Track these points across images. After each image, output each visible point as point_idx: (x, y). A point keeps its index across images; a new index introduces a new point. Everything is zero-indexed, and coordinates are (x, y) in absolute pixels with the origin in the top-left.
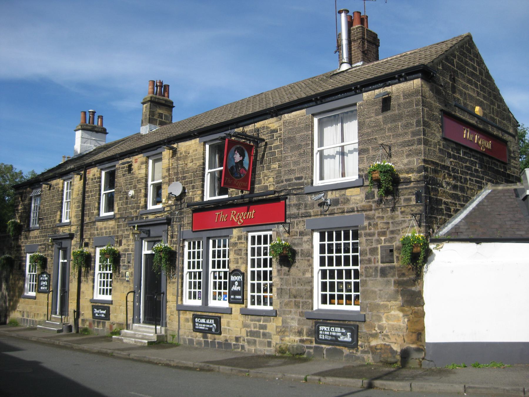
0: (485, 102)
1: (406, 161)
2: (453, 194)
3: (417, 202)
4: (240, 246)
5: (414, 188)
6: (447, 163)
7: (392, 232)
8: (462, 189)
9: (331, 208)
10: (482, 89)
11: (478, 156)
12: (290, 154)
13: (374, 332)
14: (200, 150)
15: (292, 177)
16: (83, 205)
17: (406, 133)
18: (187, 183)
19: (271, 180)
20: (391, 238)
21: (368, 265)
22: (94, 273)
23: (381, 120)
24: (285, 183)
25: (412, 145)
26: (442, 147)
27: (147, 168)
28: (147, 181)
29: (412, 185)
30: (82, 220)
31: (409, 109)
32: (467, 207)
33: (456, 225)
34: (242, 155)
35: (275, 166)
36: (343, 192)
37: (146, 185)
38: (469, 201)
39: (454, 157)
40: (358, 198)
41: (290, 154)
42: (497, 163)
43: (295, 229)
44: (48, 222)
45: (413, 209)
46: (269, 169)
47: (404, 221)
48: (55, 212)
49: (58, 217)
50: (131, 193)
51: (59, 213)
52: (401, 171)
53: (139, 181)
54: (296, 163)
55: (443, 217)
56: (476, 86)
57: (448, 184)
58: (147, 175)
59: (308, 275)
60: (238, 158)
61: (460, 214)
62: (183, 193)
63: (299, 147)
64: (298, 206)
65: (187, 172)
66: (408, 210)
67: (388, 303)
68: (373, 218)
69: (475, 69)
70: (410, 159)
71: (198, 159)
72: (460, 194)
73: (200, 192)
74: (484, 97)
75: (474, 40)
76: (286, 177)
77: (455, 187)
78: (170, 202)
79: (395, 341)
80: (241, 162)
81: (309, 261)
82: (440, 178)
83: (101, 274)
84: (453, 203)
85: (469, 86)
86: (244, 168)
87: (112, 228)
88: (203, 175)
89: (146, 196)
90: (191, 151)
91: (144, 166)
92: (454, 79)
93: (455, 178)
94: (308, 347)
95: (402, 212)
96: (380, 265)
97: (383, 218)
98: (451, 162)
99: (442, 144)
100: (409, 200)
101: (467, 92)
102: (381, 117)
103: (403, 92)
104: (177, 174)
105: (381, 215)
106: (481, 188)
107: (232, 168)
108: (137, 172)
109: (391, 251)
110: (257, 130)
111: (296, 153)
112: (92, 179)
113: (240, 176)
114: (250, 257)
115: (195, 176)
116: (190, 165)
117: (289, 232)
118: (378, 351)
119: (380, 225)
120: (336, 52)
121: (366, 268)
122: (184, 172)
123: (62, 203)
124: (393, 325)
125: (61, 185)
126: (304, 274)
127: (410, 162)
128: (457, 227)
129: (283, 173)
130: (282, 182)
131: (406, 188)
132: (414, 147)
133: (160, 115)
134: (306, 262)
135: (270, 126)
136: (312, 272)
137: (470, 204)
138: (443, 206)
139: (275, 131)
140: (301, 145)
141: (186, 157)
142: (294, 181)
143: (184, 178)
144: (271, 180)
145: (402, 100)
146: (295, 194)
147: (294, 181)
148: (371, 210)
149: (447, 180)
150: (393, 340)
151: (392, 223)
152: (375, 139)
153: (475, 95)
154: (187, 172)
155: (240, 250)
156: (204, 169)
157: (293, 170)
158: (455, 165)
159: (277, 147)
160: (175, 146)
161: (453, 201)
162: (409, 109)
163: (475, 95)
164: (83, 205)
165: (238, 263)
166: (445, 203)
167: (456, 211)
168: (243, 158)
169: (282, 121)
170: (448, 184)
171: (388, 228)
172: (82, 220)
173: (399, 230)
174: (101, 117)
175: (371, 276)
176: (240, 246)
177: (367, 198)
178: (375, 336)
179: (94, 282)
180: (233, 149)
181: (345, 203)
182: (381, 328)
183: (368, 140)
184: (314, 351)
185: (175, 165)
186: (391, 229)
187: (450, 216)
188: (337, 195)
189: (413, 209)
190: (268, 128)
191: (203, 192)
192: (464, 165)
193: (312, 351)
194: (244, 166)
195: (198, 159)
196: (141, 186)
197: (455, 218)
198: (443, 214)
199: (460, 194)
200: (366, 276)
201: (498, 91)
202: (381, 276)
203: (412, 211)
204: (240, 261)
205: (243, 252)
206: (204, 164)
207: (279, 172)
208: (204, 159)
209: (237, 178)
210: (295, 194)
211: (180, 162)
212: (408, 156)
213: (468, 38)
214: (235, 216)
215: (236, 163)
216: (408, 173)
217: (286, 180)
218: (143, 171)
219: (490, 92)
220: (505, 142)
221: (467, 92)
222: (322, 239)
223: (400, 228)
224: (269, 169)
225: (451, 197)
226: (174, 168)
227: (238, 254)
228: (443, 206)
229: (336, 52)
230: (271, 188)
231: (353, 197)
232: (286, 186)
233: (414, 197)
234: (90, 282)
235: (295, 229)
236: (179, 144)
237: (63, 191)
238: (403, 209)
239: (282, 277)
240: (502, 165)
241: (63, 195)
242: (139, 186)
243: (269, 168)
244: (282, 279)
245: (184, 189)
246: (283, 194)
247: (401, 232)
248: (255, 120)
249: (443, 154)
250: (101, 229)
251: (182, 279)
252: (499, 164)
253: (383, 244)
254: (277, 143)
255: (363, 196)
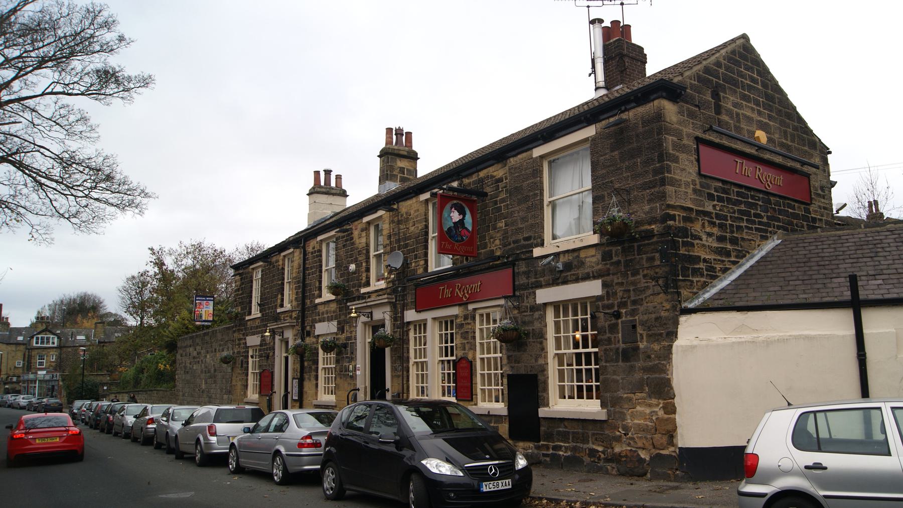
0: (771, 123)
1: (647, 208)
2: (717, 248)
3: (661, 262)
4: (467, 328)
5: (657, 242)
6: (709, 208)
7: (634, 302)
8: (734, 241)
9: (564, 274)
10: (769, 108)
11: (761, 196)
12: (517, 208)
13: (618, 433)
14: (422, 210)
15: (520, 237)
16: (304, 286)
17: (646, 172)
18: (409, 252)
19: (497, 242)
20: (633, 310)
21: (608, 347)
22: (317, 368)
23: (617, 157)
24: (512, 245)
25: (654, 187)
26: (698, 187)
27: (368, 236)
28: (368, 252)
29: (655, 239)
30: (303, 303)
31: (650, 140)
32: (743, 264)
33: (723, 289)
34: (462, 212)
35: (501, 224)
36: (576, 254)
37: (368, 258)
38: (745, 256)
39: (720, 199)
40: (594, 259)
41: (517, 208)
42: (793, 203)
43: (525, 304)
44: (269, 308)
45: (657, 270)
46: (495, 228)
47: (648, 287)
48: (277, 296)
49: (279, 301)
50: (352, 267)
51: (280, 296)
52: (639, 223)
53: (360, 253)
54: (524, 219)
55: (703, 279)
56: (758, 104)
57: (710, 235)
58: (368, 245)
59: (541, 361)
60: (456, 216)
61: (731, 274)
62: (406, 264)
63: (526, 199)
64: (527, 274)
65: (409, 238)
66: (651, 272)
67: (632, 395)
68: (612, 285)
69: (753, 80)
70: (653, 205)
71: (419, 222)
72: (729, 246)
73: (422, 262)
74: (770, 118)
75: (753, 42)
76: (514, 238)
77: (721, 239)
78: (392, 276)
79: (641, 445)
80: (461, 222)
81: (541, 343)
82: (697, 227)
83: (443, 361)
84: (719, 260)
85: (744, 103)
86: (466, 229)
87: (334, 312)
88: (427, 241)
89: (368, 270)
90: (412, 212)
91: (364, 234)
92: (718, 95)
93: (721, 226)
94: (544, 455)
95: (645, 276)
96: (622, 346)
97: (622, 284)
98: (714, 206)
99: (698, 182)
100: (652, 259)
101: (741, 112)
102: (616, 153)
103: (642, 118)
104: (398, 241)
105: (620, 281)
106: (765, 238)
107: (450, 229)
108: (357, 241)
109: (634, 327)
110: (481, 181)
111: (524, 206)
112: (312, 253)
113: (463, 240)
114: (478, 340)
115: (417, 243)
116: (412, 229)
117: (518, 308)
118: (624, 459)
119: (620, 294)
120: (590, 75)
121: (606, 350)
122: (406, 239)
123: (283, 284)
124: (639, 425)
125: (281, 263)
126: (536, 360)
127: (651, 209)
128: (723, 291)
129: (510, 233)
130: (510, 244)
131: (648, 244)
132: (657, 189)
133: (402, 170)
134: (539, 345)
135: (495, 174)
136: (546, 357)
137: (748, 261)
138: (702, 265)
139: (500, 180)
140: (529, 196)
141: (407, 220)
142: (523, 242)
143: (406, 245)
144: (497, 242)
145: (641, 130)
146: (524, 259)
147: (523, 242)
148: (608, 275)
149: (708, 230)
150: (640, 444)
151: (634, 290)
152: (611, 182)
153: (755, 116)
154: (409, 238)
155: (467, 332)
156: (427, 233)
157: (521, 228)
158: (720, 210)
159: (503, 201)
160: (395, 207)
161: (719, 258)
162: (650, 140)
163: (755, 116)
164: (304, 286)
165: (464, 349)
166: (705, 260)
167: (725, 270)
168: (464, 216)
169: (507, 168)
170: (710, 235)
171: (629, 297)
172: (303, 303)
173: (642, 299)
174: (339, 177)
175: (612, 360)
176: (467, 328)
177: (603, 259)
178: (618, 439)
179: (317, 379)
180: (448, 206)
181: (578, 267)
182: (626, 429)
183: (603, 184)
184: (551, 460)
185: (396, 230)
186: (632, 298)
187: (714, 277)
188: (571, 258)
189: (657, 270)
190: (492, 177)
191: (426, 261)
192: (736, 208)
193: (548, 459)
194: (466, 225)
195: (419, 222)
196: (362, 258)
197: (721, 280)
198: (702, 275)
199: (729, 246)
200: (606, 362)
201: (794, 108)
202: (623, 361)
203: (657, 273)
204: (467, 347)
205: (470, 335)
206: (427, 227)
207: (506, 232)
208: (427, 220)
209: (457, 241)
210: (524, 259)
211: (402, 227)
212: (650, 201)
213: (742, 41)
214: (460, 290)
215: (454, 223)
216: (650, 224)
217: (514, 242)
218: (364, 240)
219: (780, 111)
220: (808, 176)
221: (741, 112)
222: (557, 315)
223: (643, 296)
224: (495, 228)
225: (715, 252)
226: (395, 234)
227: (465, 338)
228: (702, 265)
229: (590, 75)
230: (498, 253)
231: (588, 260)
232: (513, 249)
233: (657, 255)
234: (313, 379)
235: (525, 304)
236: (401, 204)
237: (283, 269)
238: (645, 272)
239: (513, 365)
240: (802, 206)
241: (283, 274)
242: (360, 259)
243: (495, 228)
244: (512, 367)
245: (405, 259)
246: (510, 259)
247: (644, 302)
248: (479, 168)
249: (700, 196)
250: (323, 314)
251: (408, 371)
252: (796, 205)
253: (624, 319)
254: (503, 196)
255: (599, 257)
